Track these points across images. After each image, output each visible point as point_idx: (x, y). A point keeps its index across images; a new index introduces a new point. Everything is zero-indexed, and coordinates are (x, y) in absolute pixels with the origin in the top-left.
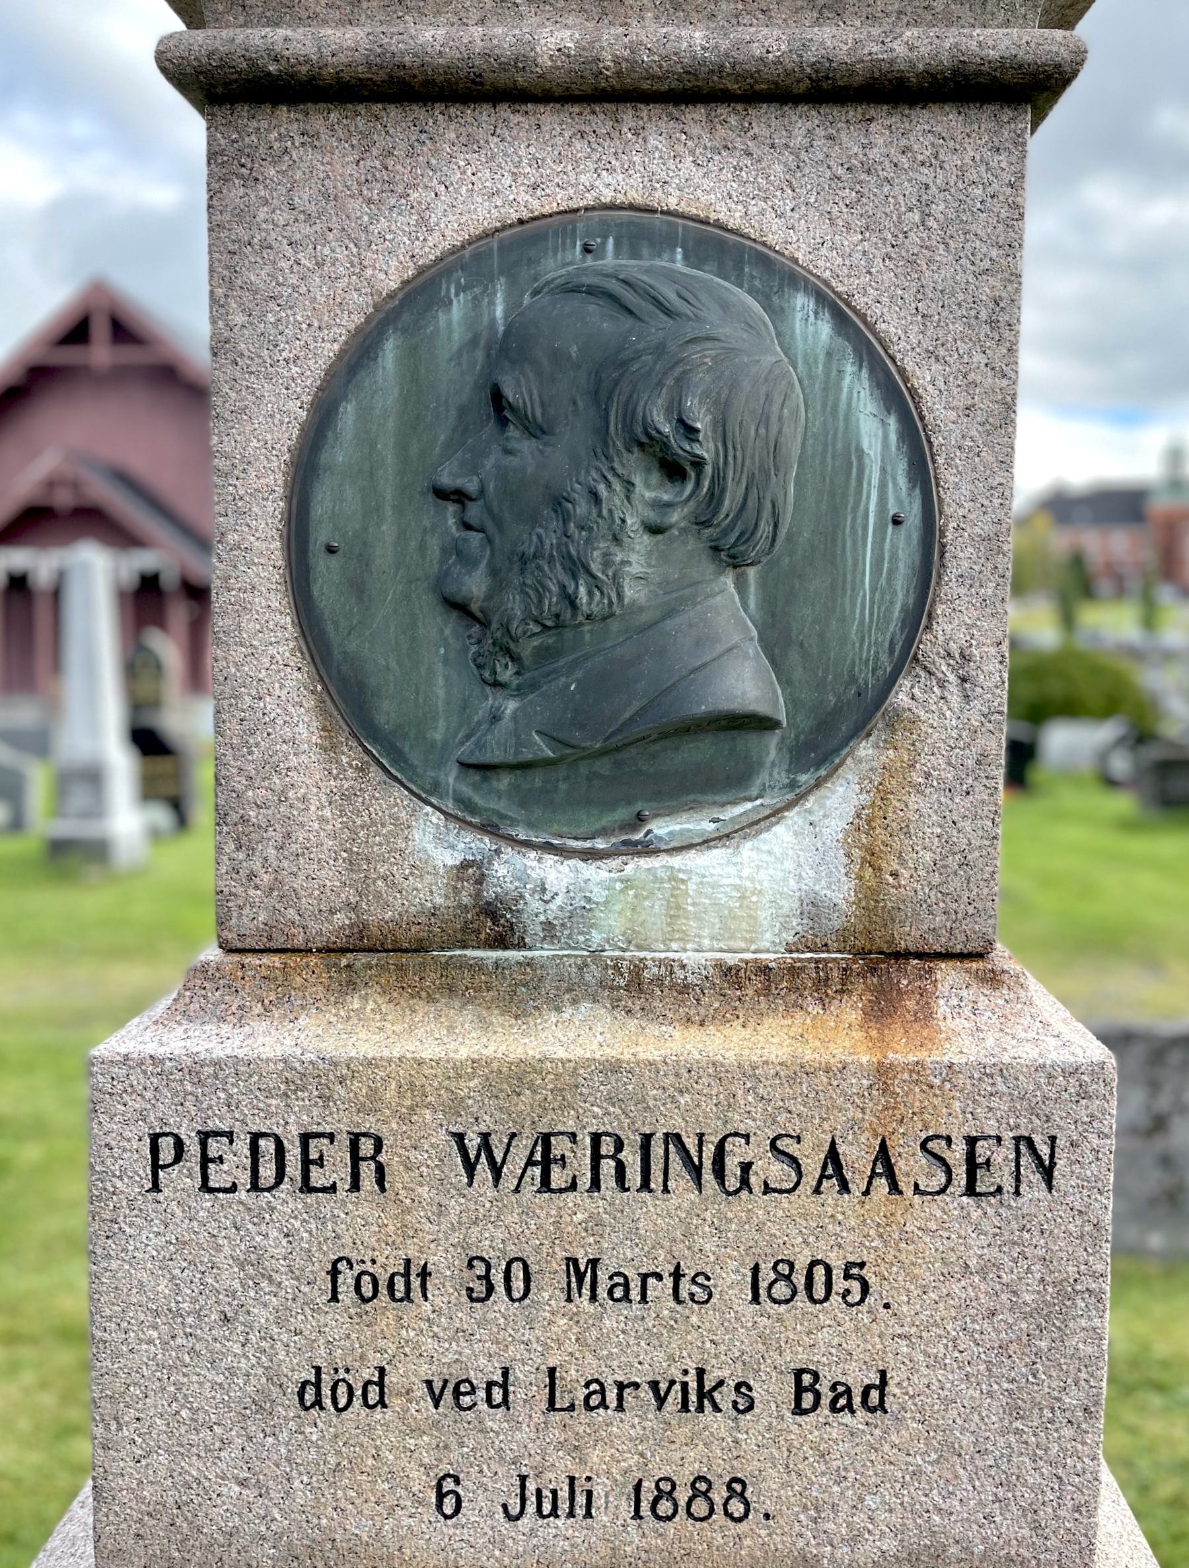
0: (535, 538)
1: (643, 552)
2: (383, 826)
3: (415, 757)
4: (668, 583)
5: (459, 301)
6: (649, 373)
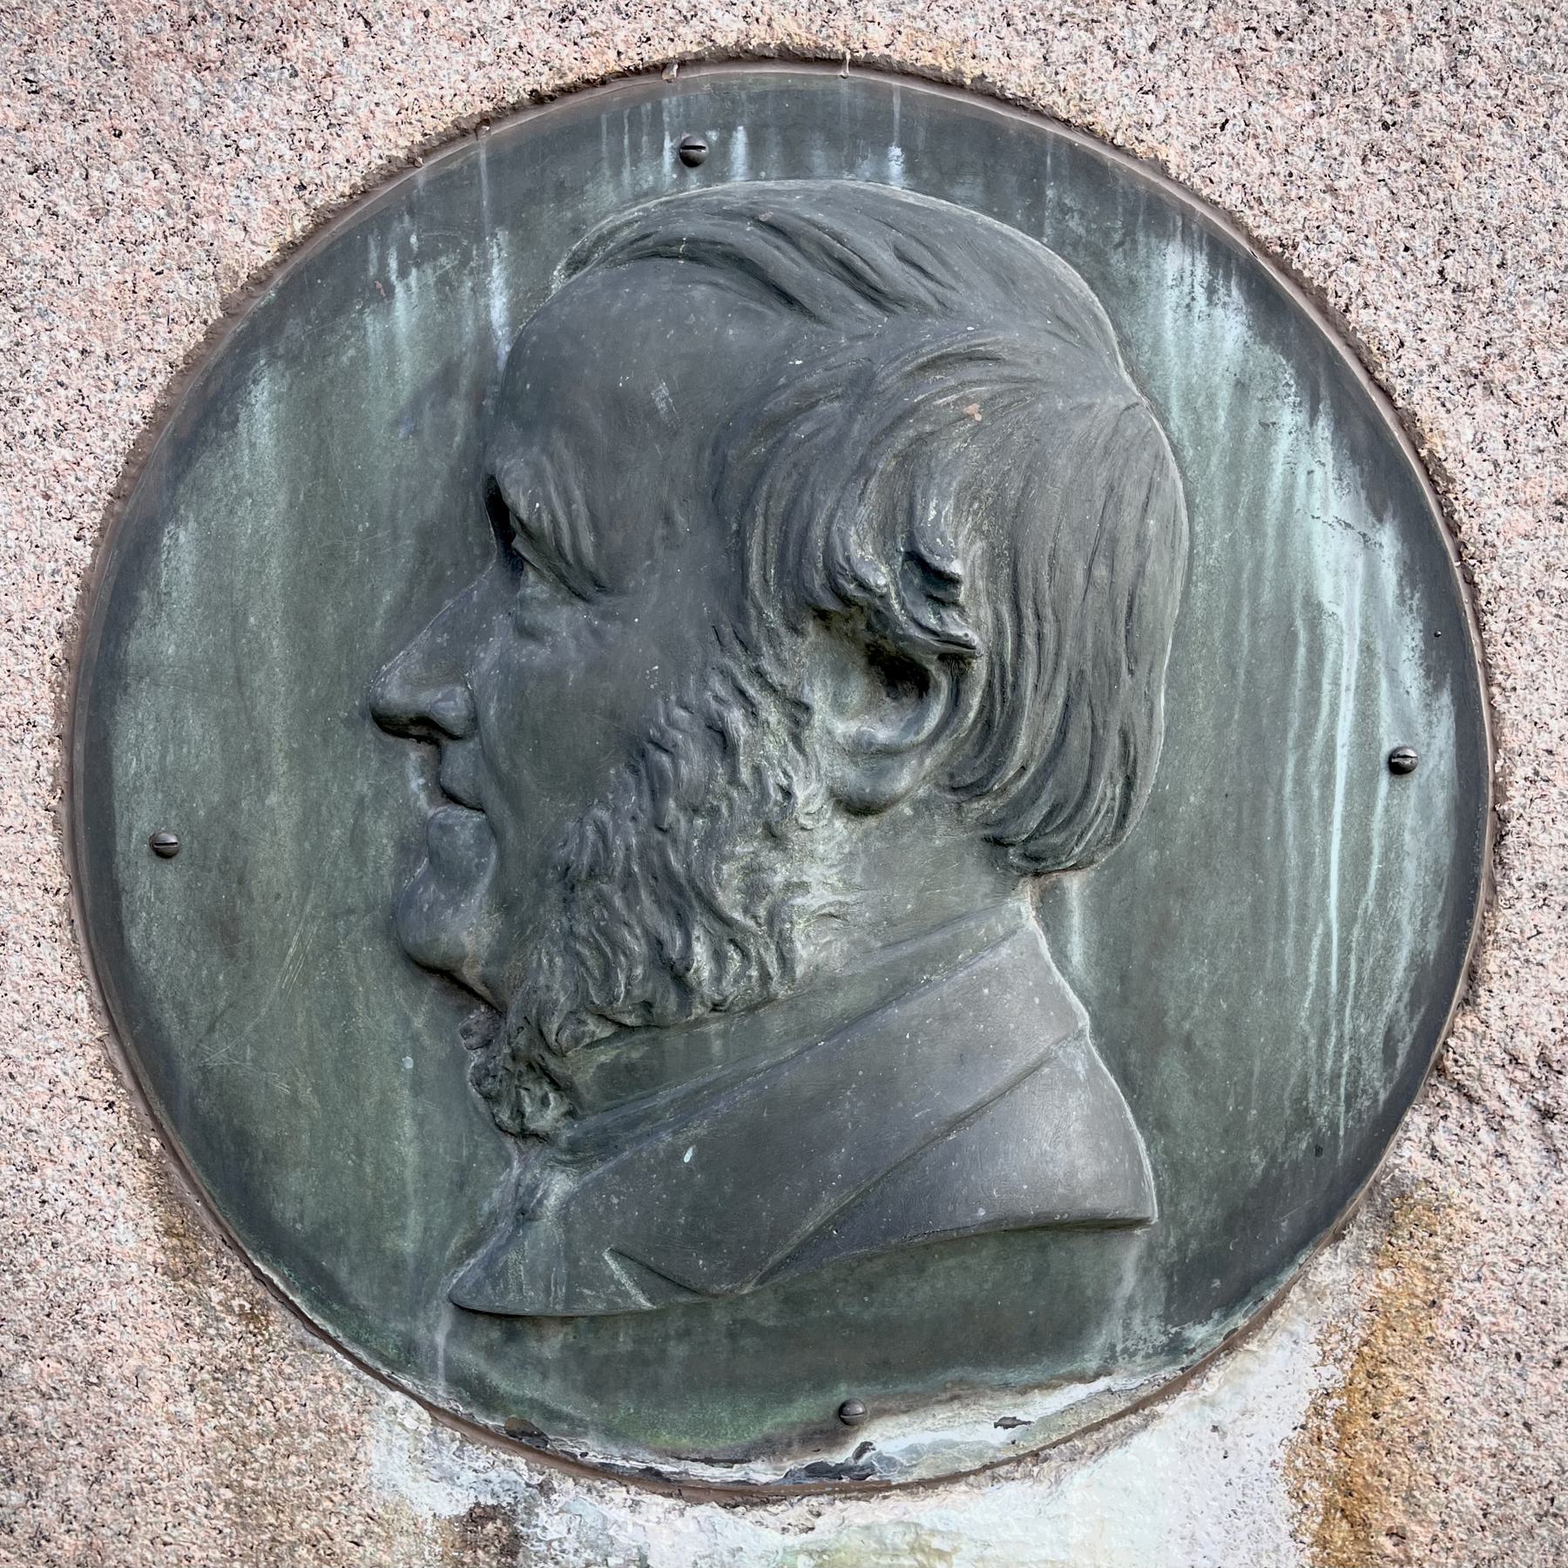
0: (590, 830)
1: (834, 856)
2: (304, 1433)
3: (361, 1290)
4: (891, 924)
5: (408, 288)
6: (838, 443)
